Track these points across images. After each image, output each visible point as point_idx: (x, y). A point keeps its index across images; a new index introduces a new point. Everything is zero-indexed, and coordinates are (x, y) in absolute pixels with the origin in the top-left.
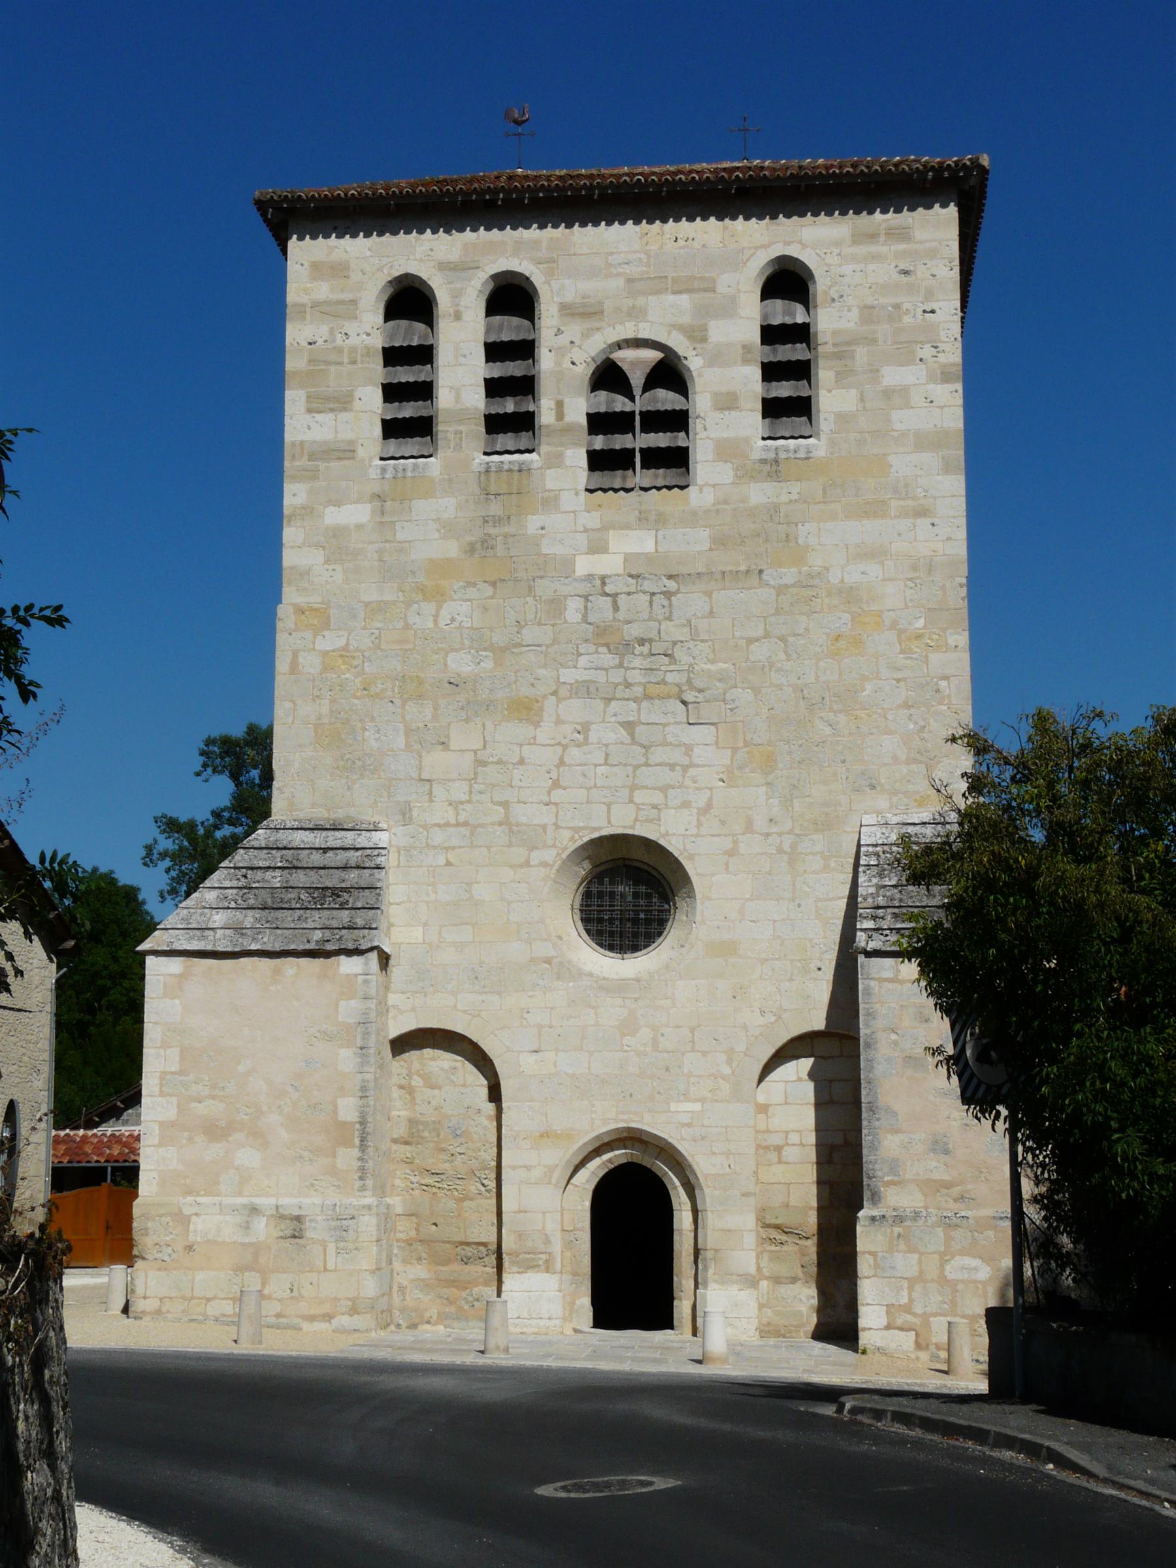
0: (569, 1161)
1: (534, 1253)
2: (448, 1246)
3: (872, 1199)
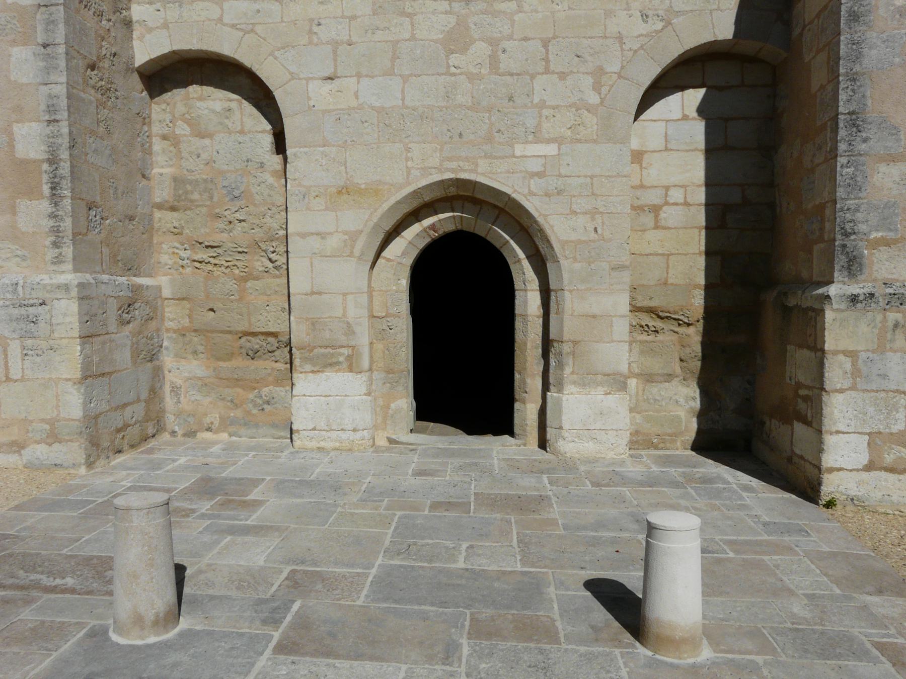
0: (377, 226)
1: (333, 348)
2: (229, 336)
3: (849, 269)
